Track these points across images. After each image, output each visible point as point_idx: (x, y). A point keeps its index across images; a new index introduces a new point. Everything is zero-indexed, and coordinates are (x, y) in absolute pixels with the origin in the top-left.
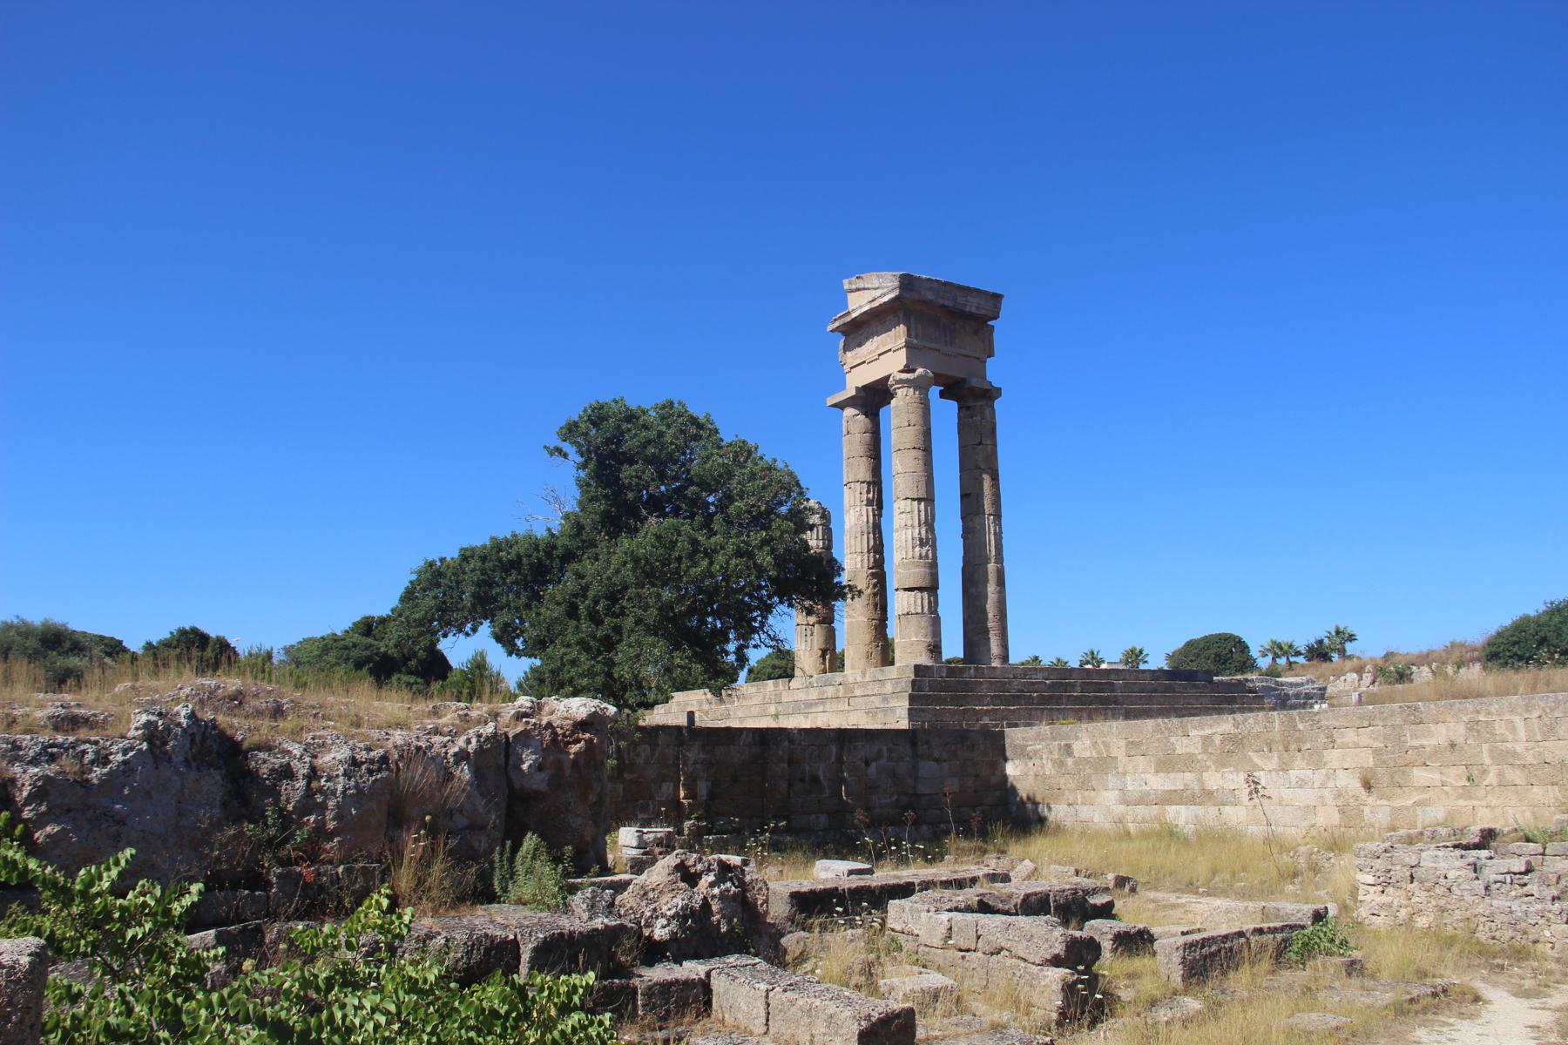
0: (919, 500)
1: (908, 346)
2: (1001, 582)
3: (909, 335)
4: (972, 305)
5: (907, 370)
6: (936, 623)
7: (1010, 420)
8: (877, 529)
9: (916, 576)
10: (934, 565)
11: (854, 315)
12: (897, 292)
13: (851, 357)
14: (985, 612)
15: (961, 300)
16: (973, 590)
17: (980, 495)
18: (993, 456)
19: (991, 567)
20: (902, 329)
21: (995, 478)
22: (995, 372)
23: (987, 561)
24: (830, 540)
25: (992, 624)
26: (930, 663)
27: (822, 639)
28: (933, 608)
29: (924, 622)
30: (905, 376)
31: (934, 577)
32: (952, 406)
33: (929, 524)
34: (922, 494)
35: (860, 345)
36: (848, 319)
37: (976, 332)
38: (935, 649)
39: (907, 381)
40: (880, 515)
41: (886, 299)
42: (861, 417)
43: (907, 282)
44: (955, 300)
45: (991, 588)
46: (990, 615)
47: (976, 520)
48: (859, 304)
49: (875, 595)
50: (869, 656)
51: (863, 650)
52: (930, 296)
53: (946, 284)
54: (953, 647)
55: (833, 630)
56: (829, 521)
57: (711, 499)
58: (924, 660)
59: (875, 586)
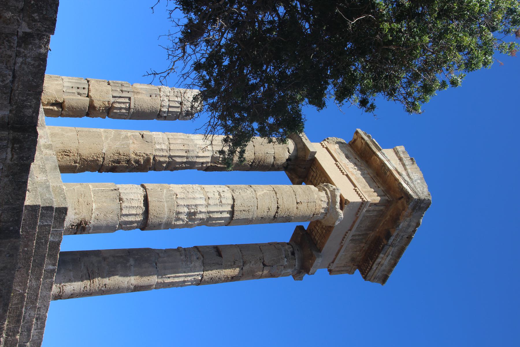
0: (232, 213)
1: (363, 203)
2: (137, 288)
3: (372, 204)
4: (383, 260)
5: (344, 202)
6: (110, 228)
7: (283, 287)
8: (190, 165)
9: (160, 209)
10: (168, 225)
11: (379, 153)
12: (415, 197)
13: (335, 148)
14: (110, 274)
15: (392, 250)
16: (132, 262)
17: (220, 266)
18: (251, 275)
19: (154, 279)
20: (376, 199)
21: (233, 279)
22: (319, 276)
23: (160, 274)
24: (165, 118)
25: (98, 282)
26: (67, 223)
27: (74, 104)
28: (125, 226)
29: (112, 218)
30: (338, 199)
31: (157, 226)
32: (286, 238)
33: (209, 221)
34: (237, 215)
35: (347, 157)
36: (374, 149)
37: (353, 260)
38: (81, 228)
39: (334, 202)
40: (199, 169)
41: (405, 185)
42: (287, 156)
43: (421, 206)
44: (392, 245)
45: (133, 280)
46: (106, 281)
47: (198, 263)
48: (389, 157)
49: (128, 161)
50: (66, 153)
51: (72, 146)
52: (403, 224)
53: (410, 238)
54: (70, 244)
55: (81, 116)
56: (184, 118)
57: (426, 39)
58: (71, 218)
59: (137, 162)
